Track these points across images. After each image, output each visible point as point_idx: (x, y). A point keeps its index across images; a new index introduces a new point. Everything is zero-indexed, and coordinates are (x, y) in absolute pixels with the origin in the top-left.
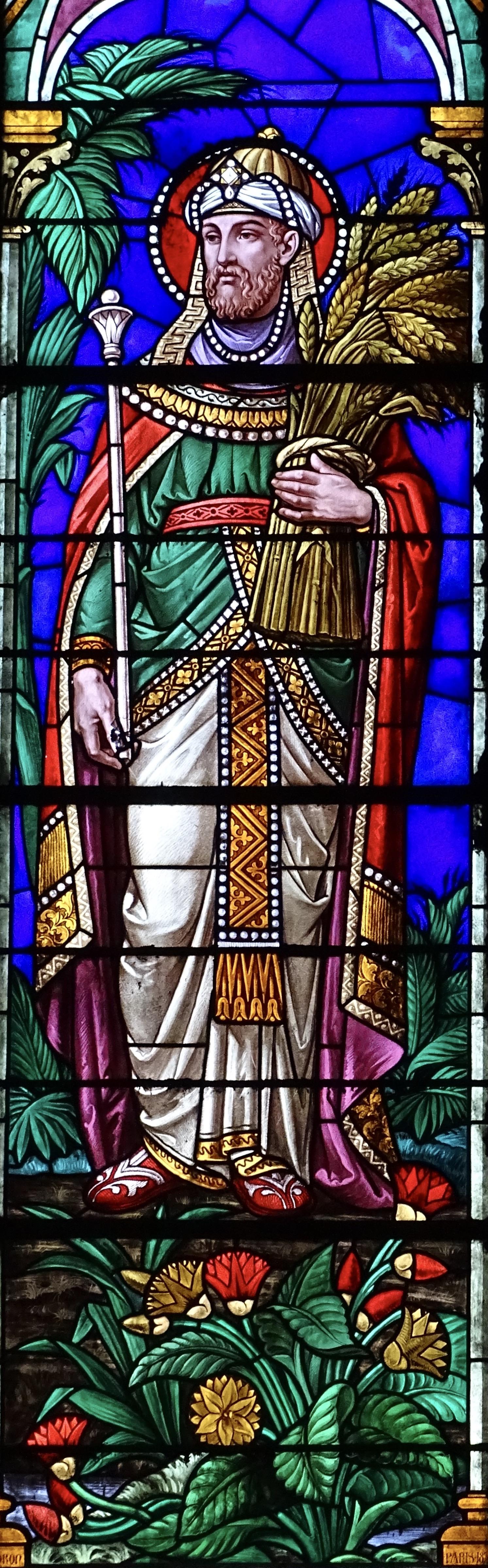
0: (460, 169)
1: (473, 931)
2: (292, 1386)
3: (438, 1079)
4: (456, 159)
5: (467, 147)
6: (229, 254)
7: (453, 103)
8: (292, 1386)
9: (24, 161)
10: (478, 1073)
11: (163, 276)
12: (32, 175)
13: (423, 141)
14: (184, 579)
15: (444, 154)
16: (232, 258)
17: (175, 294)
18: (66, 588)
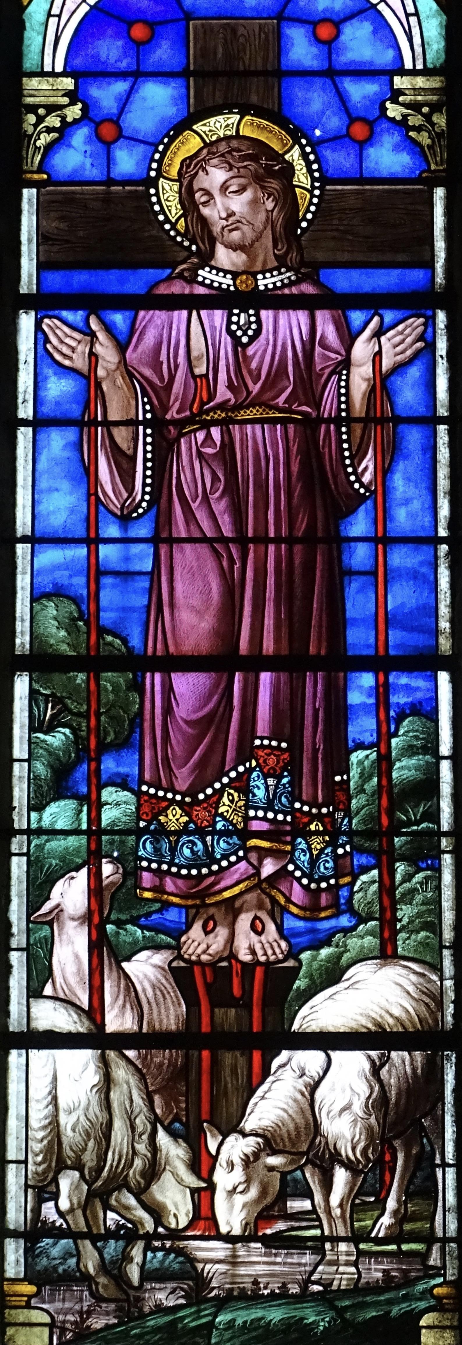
0: (418, 129)
2: (160, 624)
5: (425, 110)
6: (227, 209)
7: (414, 73)
8: (160, 624)
9: (40, 119)
10: (446, 825)
12: (49, 130)
15: (405, 117)
16: (230, 212)
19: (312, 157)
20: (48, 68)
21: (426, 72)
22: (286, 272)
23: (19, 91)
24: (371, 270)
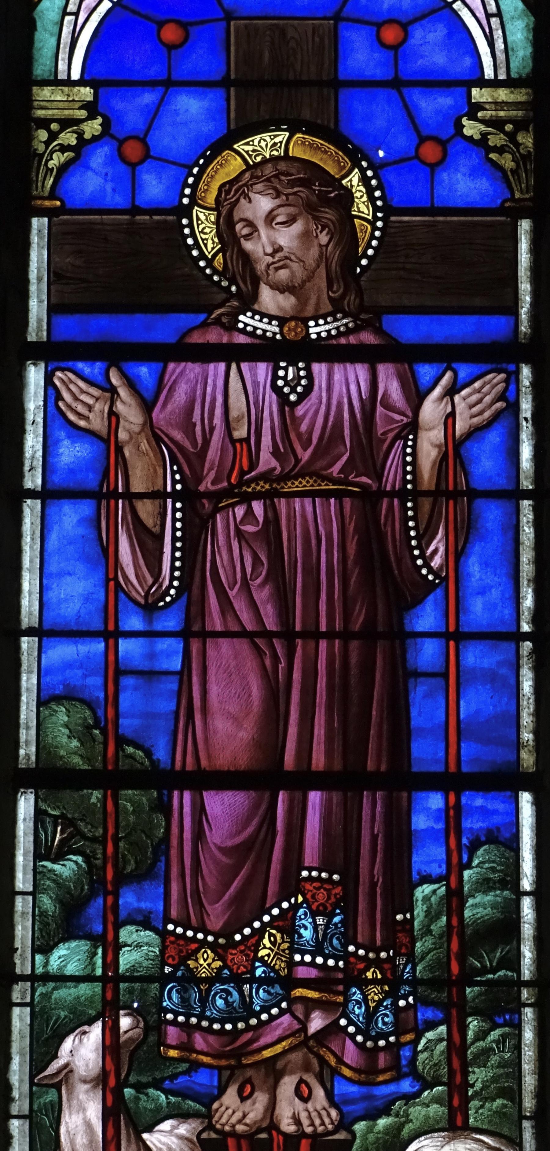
1: (456, 317)
3: (499, 374)
4: (496, 140)
5: (509, 127)
6: (273, 243)
7: (495, 83)
9: (53, 136)
11: (427, 575)
12: (63, 149)
13: (465, 121)
14: (263, 564)
15: (484, 136)
16: (276, 247)
17: (427, 575)
18: (290, 605)
21: (510, 83)
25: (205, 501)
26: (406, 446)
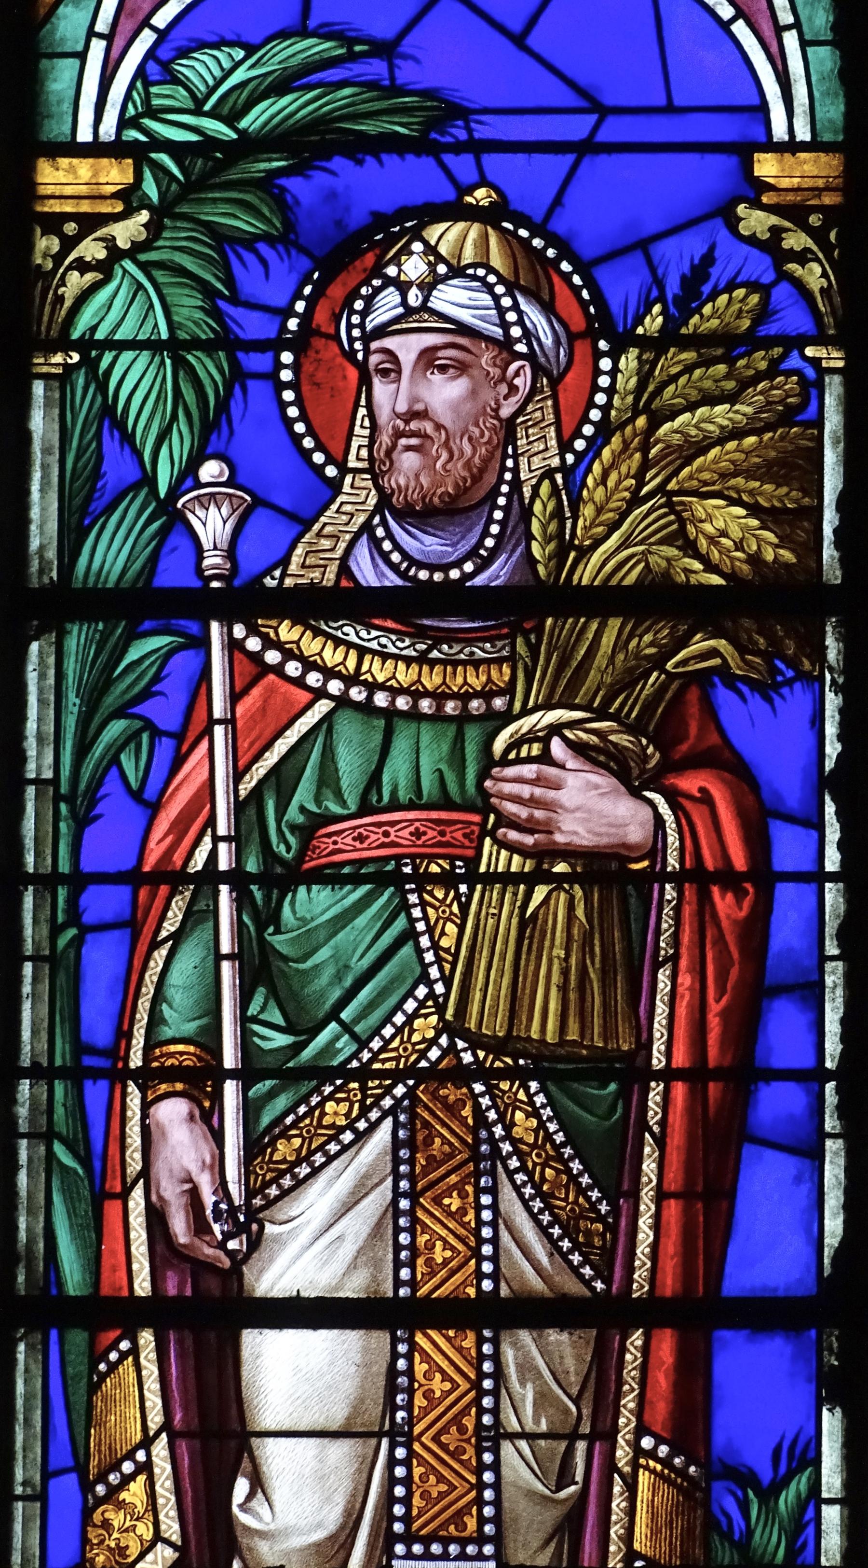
4: (796, 240)
6: (414, 400)
7: (792, 146)
9: (69, 244)
12: (82, 266)
13: (741, 209)
15: (776, 232)
16: (419, 407)
19: (546, 1218)
20: (84, 135)
21: (814, 146)
22: (627, 1383)
23: (28, 188)
24: (244, 1384)
25: (254, 888)
26: (606, 409)
